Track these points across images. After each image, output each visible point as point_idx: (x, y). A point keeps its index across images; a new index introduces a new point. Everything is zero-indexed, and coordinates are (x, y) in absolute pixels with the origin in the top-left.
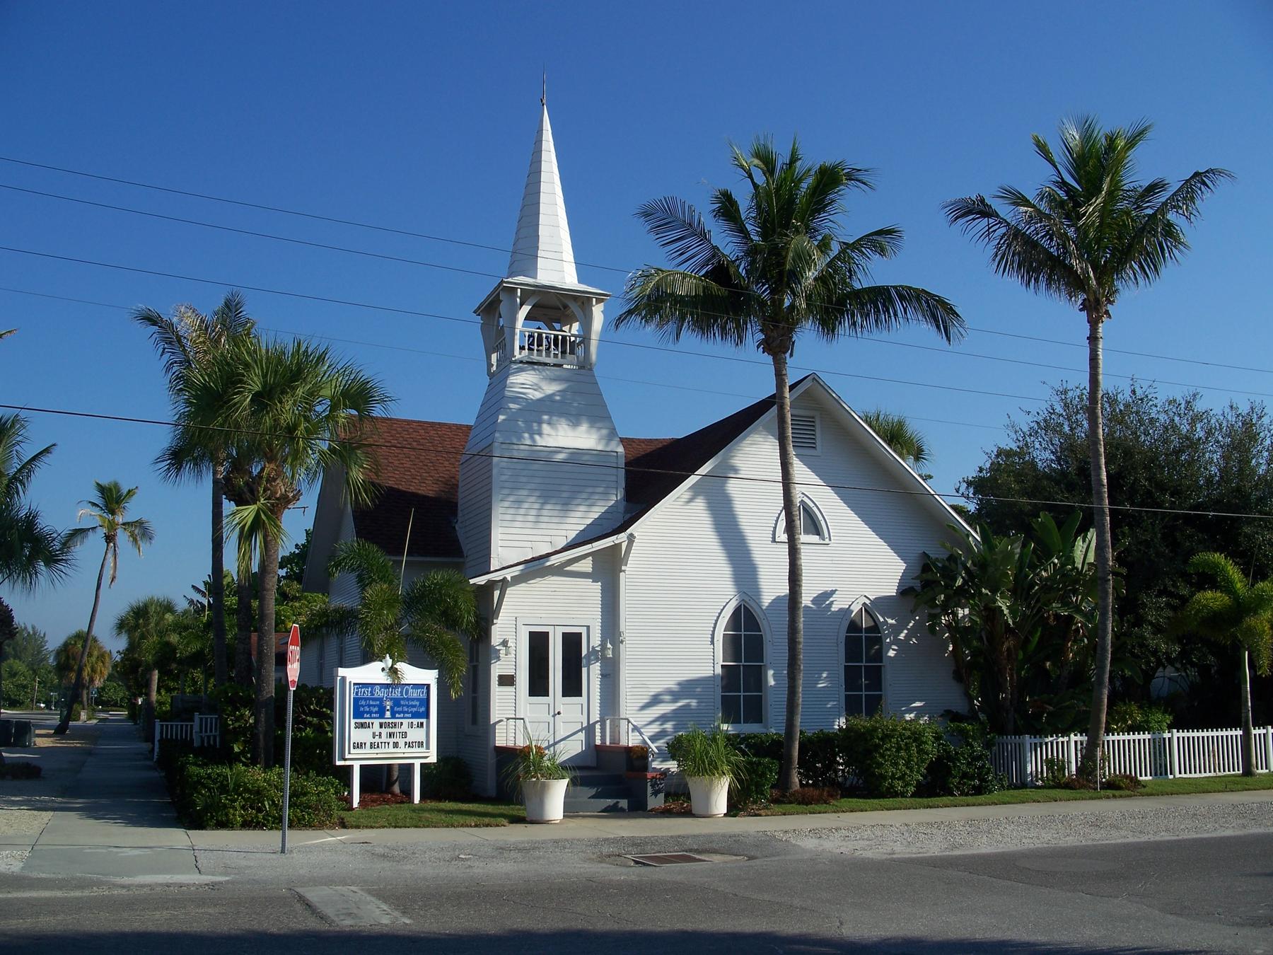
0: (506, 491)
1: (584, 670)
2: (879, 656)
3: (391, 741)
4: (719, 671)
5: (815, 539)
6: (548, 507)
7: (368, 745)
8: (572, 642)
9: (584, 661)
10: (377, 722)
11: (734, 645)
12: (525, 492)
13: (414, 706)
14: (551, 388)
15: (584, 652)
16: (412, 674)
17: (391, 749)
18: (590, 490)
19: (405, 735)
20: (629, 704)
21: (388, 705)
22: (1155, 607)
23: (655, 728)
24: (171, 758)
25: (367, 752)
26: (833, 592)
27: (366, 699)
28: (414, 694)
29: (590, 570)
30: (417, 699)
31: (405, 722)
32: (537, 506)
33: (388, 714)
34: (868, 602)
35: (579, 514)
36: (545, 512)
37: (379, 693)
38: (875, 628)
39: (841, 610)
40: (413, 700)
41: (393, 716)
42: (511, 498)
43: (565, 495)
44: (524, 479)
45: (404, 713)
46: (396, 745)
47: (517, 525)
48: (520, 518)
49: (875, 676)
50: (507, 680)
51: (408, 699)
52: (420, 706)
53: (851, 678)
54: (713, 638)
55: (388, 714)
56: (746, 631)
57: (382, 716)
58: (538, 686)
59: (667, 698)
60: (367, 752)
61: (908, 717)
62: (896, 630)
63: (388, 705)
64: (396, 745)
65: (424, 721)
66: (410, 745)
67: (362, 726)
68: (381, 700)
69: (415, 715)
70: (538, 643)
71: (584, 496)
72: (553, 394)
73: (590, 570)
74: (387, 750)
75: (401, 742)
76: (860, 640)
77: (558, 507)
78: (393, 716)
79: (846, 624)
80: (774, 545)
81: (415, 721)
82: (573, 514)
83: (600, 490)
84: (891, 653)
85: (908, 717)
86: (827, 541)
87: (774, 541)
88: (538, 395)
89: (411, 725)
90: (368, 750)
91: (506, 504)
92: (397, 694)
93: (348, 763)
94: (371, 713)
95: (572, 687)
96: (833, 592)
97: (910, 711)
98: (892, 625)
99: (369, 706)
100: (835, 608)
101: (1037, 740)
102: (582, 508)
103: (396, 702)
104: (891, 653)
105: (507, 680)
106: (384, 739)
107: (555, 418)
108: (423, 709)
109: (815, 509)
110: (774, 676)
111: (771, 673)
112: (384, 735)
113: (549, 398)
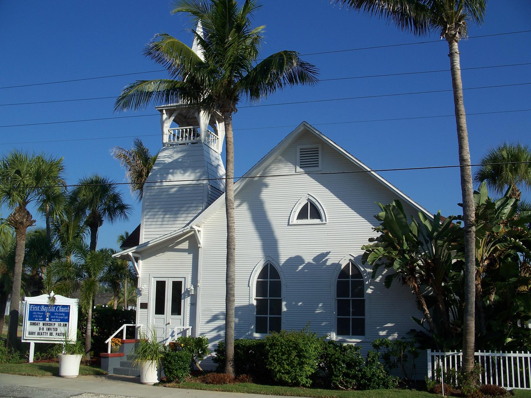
0: (147, 210)
1: (182, 301)
2: (362, 292)
3: (49, 332)
4: (255, 303)
5: (317, 221)
6: (167, 216)
7: (36, 333)
8: (177, 286)
9: (183, 296)
10: (41, 323)
11: (261, 288)
12: (156, 210)
13: (62, 316)
14: (177, 156)
15: (183, 292)
16: (61, 300)
17: (48, 336)
18: (188, 205)
19: (56, 329)
20: (201, 319)
21: (48, 315)
22: (50, 220)
23: (214, 334)
24: (176, 347)
25: (36, 336)
26: (328, 253)
27: (36, 312)
28: (62, 310)
29: (187, 248)
30: (64, 313)
31: (57, 323)
32: (162, 216)
33: (47, 319)
34: (352, 258)
35: (182, 219)
36: (166, 219)
37: (43, 309)
38: (358, 274)
39: (333, 264)
40: (61, 313)
41: (50, 320)
42: (150, 214)
43: (175, 209)
44: (156, 204)
45: (56, 319)
46: (51, 334)
47: (153, 226)
48: (154, 223)
49: (360, 306)
50: (144, 306)
51: (58, 312)
52: (65, 316)
53: (342, 307)
54: (249, 283)
55: (47, 319)
56: (271, 281)
57: (44, 320)
58: (160, 309)
59: (222, 317)
60: (36, 336)
61: (382, 333)
62: (373, 276)
63: (48, 315)
64: (51, 334)
65: (67, 323)
66: (59, 335)
67: (34, 324)
68: (44, 312)
69: (62, 320)
70: (161, 286)
71: (185, 209)
72: (179, 159)
73: (187, 248)
74: (46, 336)
75: (54, 333)
76: (348, 284)
77: (172, 216)
78: (50, 320)
79: (337, 273)
80: (290, 227)
81: (62, 323)
82: (179, 219)
83: (194, 205)
84: (369, 291)
85: (382, 333)
86: (324, 222)
87: (289, 225)
88: (170, 160)
89: (60, 325)
90: (36, 336)
91: (148, 217)
92: (53, 310)
93: (28, 341)
94: (39, 318)
95: (176, 310)
96: (328, 253)
97: (383, 329)
98: (369, 273)
99: (38, 315)
100: (329, 263)
101: (440, 354)
102: (184, 215)
103: (52, 314)
104: (369, 291)
105: (144, 306)
106: (45, 330)
107: (175, 171)
108: (67, 317)
109: (317, 203)
110: (286, 305)
111: (284, 303)
112: (45, 329)
113: (176, 161)
